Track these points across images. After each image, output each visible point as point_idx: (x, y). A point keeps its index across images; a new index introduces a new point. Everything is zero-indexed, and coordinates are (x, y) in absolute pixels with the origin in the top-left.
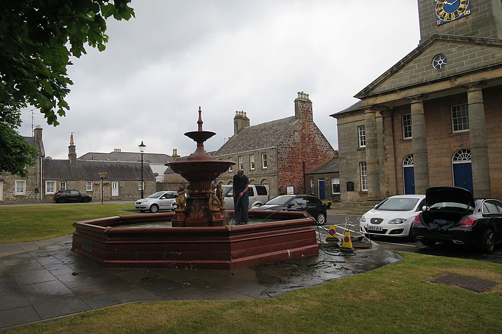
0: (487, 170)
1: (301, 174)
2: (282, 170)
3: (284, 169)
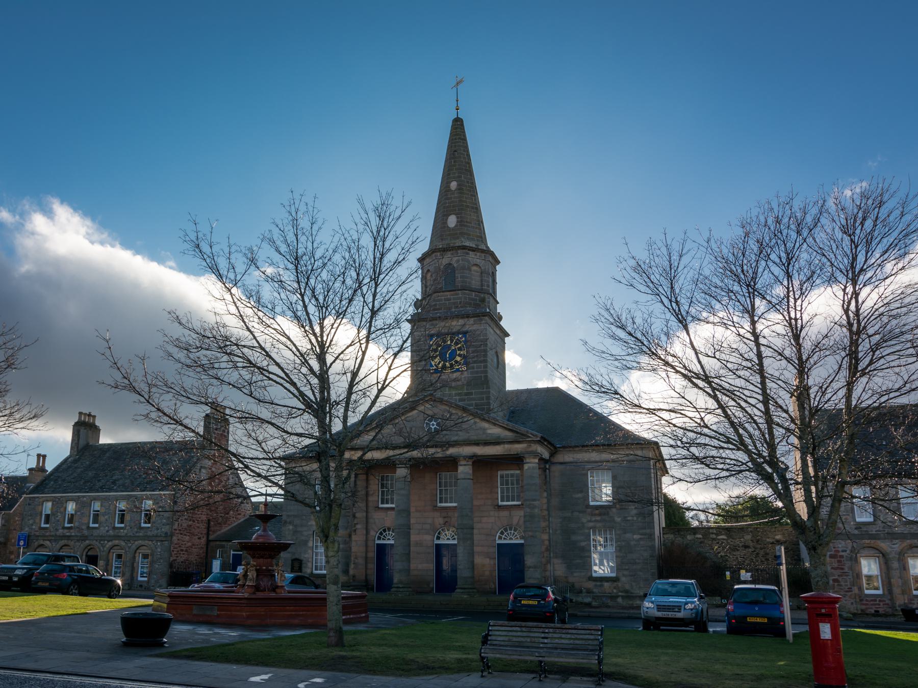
0: (471, 554)
1: (203, 540)
2: (178, 531)
3: (180, 530)
